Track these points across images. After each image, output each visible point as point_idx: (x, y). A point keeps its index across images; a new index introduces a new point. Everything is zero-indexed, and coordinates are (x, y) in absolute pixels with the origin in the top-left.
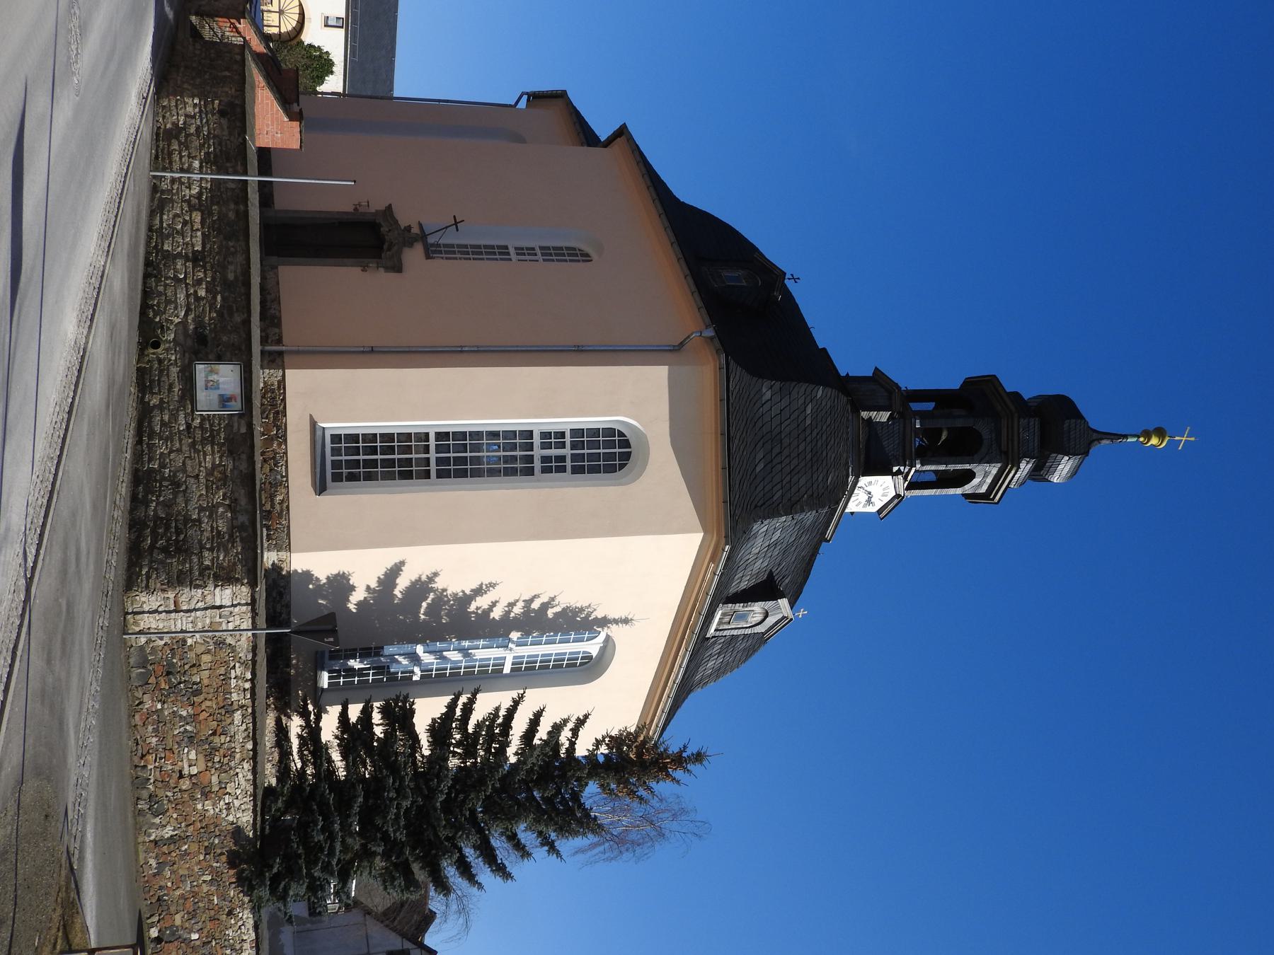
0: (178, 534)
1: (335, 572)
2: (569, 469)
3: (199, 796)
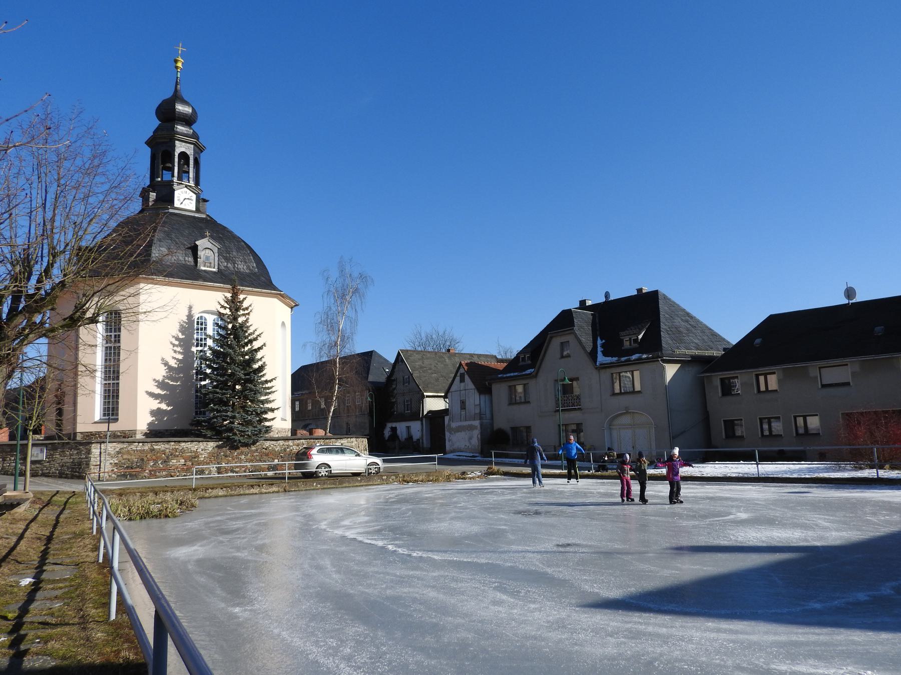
0: (76, 465)
1: (150, 415)
2: (119, 333)
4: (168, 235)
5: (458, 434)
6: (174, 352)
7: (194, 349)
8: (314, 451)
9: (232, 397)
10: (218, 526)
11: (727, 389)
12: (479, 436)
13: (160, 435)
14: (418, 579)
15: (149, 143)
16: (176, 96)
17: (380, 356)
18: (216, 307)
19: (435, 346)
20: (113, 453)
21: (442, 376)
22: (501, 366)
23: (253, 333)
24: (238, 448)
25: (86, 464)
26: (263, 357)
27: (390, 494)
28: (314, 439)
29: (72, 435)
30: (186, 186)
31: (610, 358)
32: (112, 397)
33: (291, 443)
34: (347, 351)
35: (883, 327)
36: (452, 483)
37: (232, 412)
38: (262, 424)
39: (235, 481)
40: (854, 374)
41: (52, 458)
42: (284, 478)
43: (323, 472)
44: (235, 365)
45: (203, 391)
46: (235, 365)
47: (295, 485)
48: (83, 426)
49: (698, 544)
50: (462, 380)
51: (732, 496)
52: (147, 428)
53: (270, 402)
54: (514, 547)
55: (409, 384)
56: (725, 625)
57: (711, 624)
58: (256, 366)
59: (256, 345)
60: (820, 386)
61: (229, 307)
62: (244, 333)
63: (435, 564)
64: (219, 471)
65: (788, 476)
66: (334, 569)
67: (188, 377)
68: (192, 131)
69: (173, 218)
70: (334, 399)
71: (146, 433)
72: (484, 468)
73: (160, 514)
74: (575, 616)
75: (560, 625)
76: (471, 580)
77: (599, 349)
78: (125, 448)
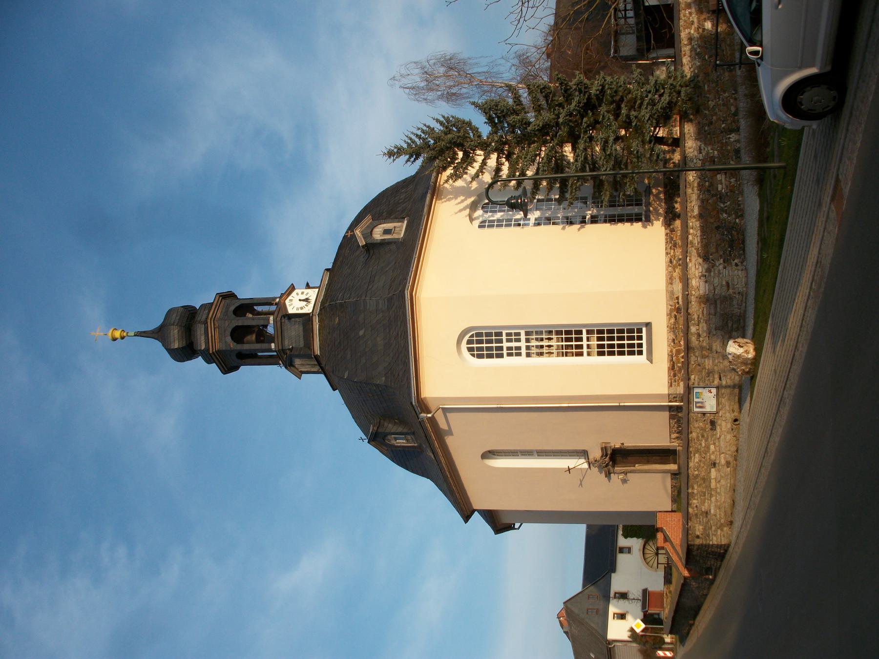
3: (716, 160)
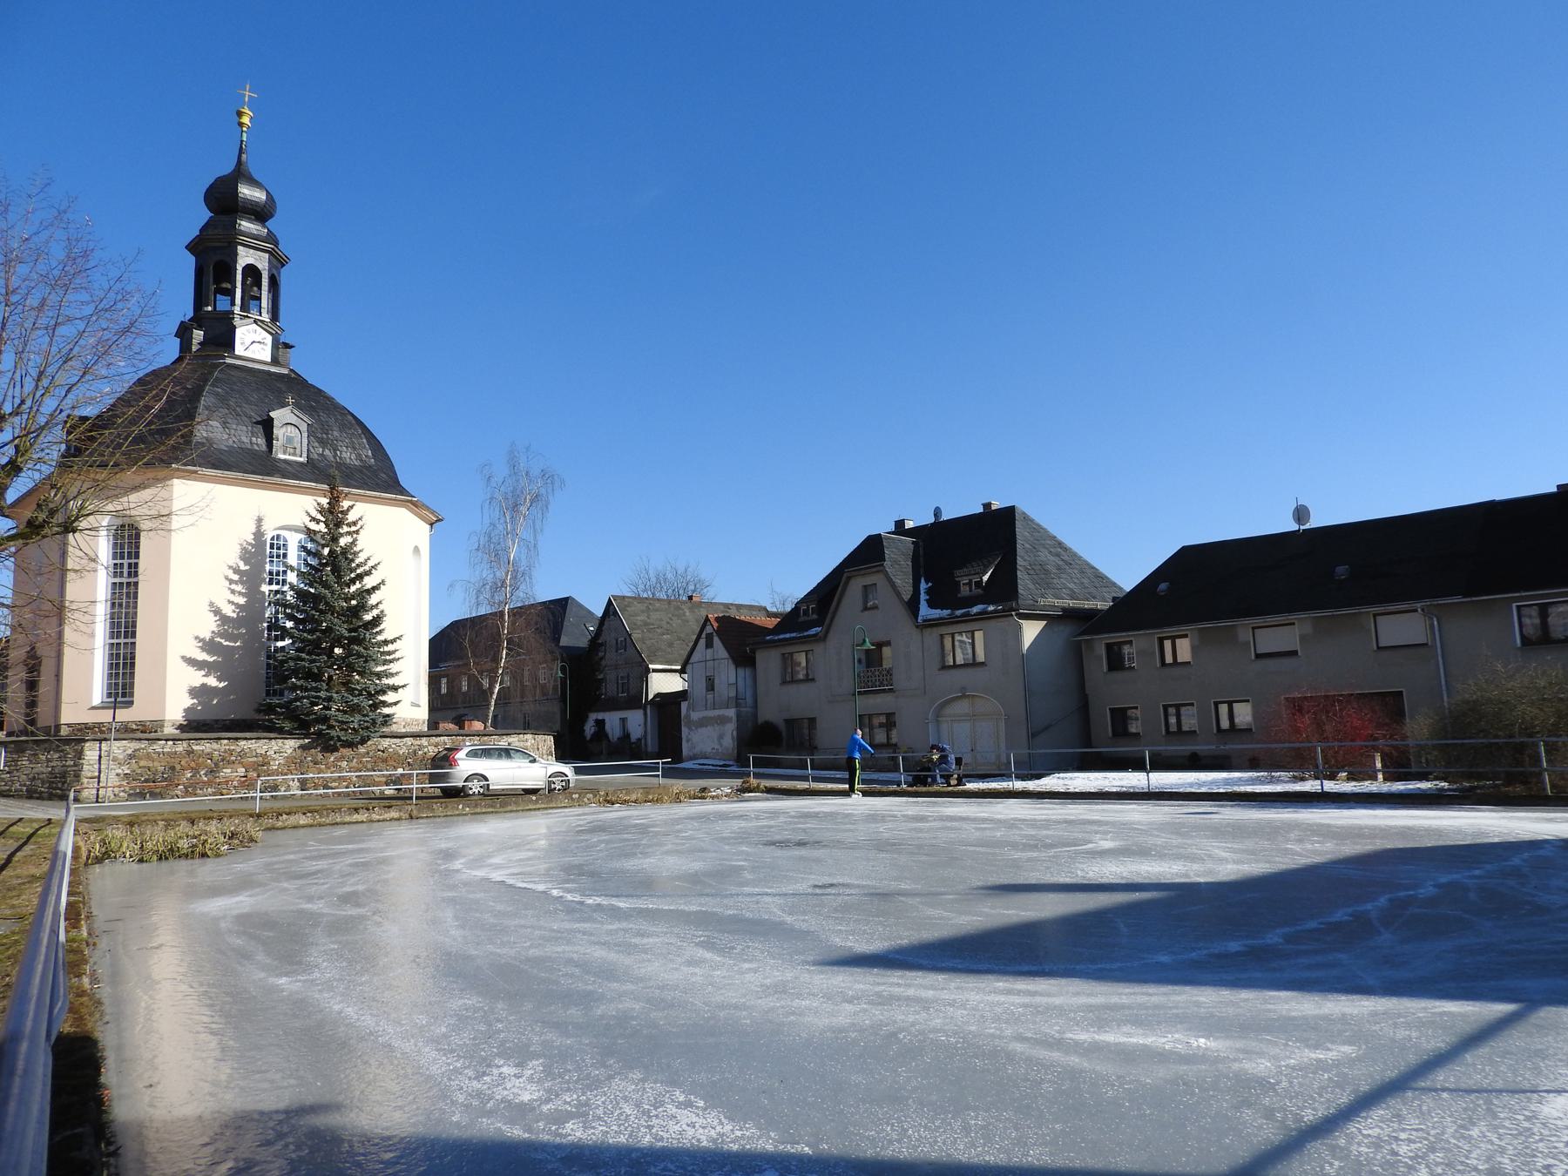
2: (136, 561)
4: (223, 400)
5: (703, 730)
6: (232, 593)
7: (265, 588)
8: (461, 755)
9: (328, 667)
10: (287, 868)
11: (1116, 661)
12: (735, 733)
13: (205, 728)
14: (584, 933)
15: (192, 247)
16: (239, 171)
17: (581, 606)
18: (301, 520)
19: (670, 591)
20: (121, 757)
21: (679, 639)
22: (771, 623)
23: (365, 563)
24: (337, 750)
25: (75, 776)
26: (380, 602)
27: (581, 820)
28: (462, 736)
29: (53, 730)
30: (255, 321)
31: (938, 611)
32: (122, 668)
33: (424, 741)
34: (521, 594)
35: (1347, 567)
36: (682, 804)
37: (327, 690)
38: (379, 711)
39: (328, 803)
40: (1303, 638)
41: (16, 765)
42: (411, 798)
43: (475, 787)
44: (332, 614)
45: (280, 656)
46: (332, 614)
47: (428, 807)
48: (71, 714)
49: (1026, 882)
50: (709, 645)
51: (1102, 819)
52: (183, 717)
53: (392, 675)
54: (747, 890)
55: (625, 650)
56: (1022, 984)
57: (1001, 983)
58: (368, 617)
59: (369, 582)
60: (1253, 657)
61: (324, 520)
62: (349, 564)
63: (615, 913)
64: (303, 785)
65: (1193, 790)
66: (456, 923)
67: (254, 634)
68: (266, 231)
69: (233, 373)
70: (500, 672)
71: (181, 724)
72: (738, 782)
73: (192, 852)
74: (805, 977)
75: (780, 989)
76: (666, 933)
77: (923, 597)
78: (143, 749)
